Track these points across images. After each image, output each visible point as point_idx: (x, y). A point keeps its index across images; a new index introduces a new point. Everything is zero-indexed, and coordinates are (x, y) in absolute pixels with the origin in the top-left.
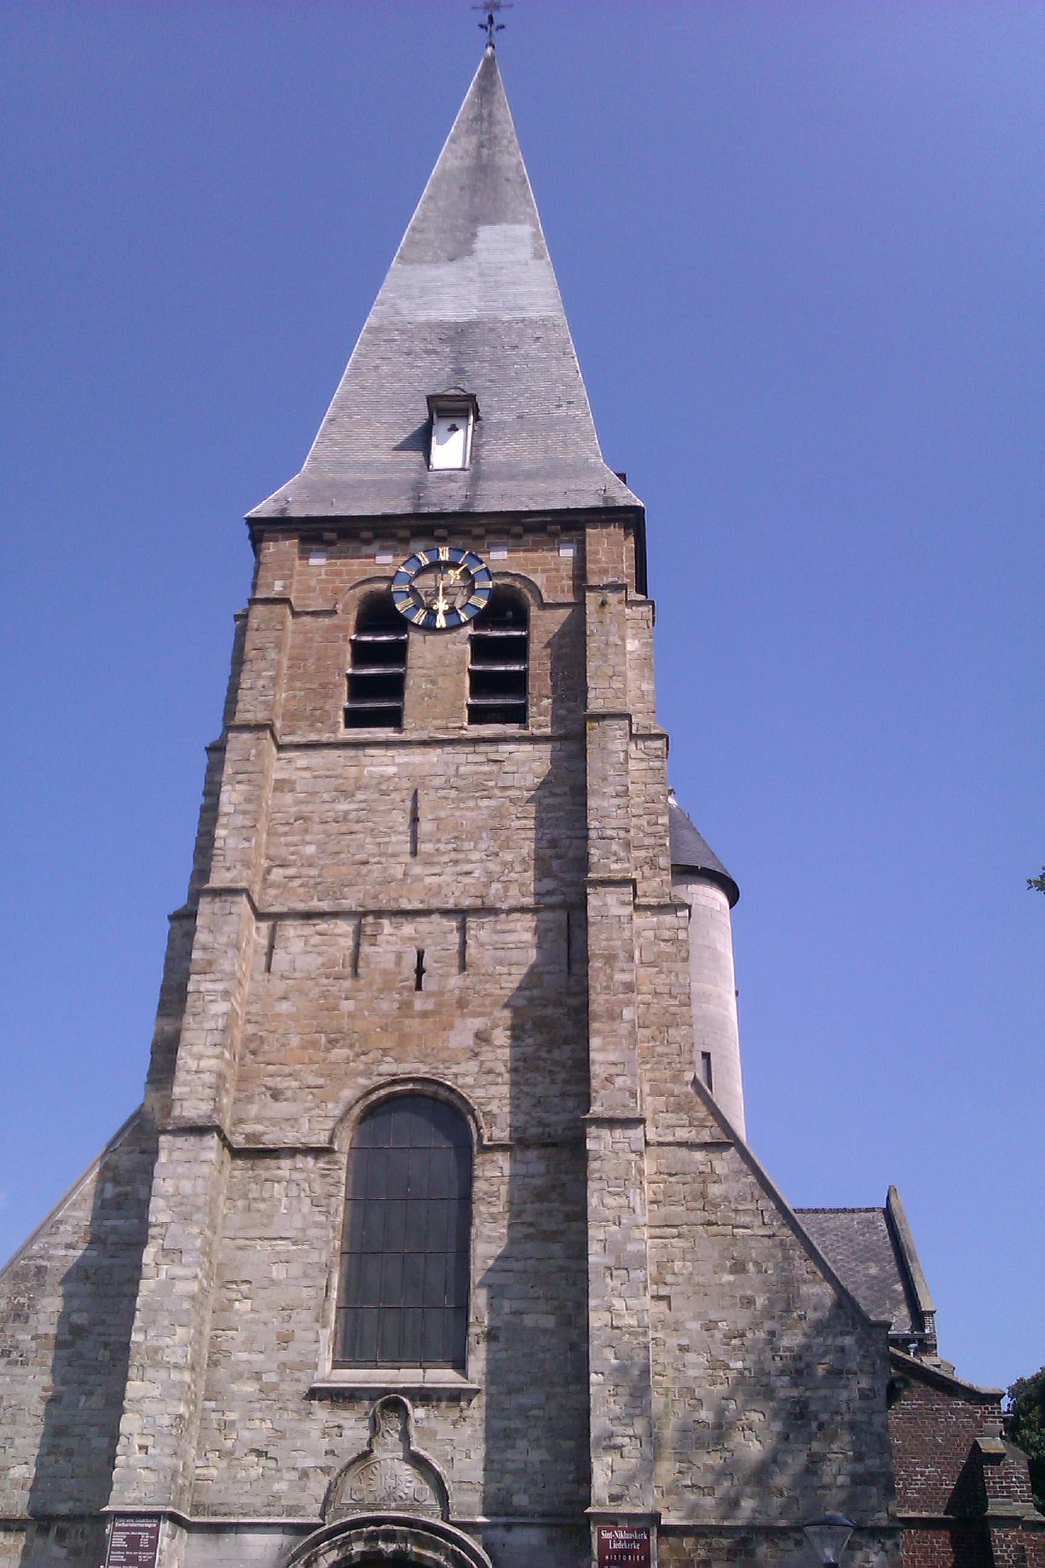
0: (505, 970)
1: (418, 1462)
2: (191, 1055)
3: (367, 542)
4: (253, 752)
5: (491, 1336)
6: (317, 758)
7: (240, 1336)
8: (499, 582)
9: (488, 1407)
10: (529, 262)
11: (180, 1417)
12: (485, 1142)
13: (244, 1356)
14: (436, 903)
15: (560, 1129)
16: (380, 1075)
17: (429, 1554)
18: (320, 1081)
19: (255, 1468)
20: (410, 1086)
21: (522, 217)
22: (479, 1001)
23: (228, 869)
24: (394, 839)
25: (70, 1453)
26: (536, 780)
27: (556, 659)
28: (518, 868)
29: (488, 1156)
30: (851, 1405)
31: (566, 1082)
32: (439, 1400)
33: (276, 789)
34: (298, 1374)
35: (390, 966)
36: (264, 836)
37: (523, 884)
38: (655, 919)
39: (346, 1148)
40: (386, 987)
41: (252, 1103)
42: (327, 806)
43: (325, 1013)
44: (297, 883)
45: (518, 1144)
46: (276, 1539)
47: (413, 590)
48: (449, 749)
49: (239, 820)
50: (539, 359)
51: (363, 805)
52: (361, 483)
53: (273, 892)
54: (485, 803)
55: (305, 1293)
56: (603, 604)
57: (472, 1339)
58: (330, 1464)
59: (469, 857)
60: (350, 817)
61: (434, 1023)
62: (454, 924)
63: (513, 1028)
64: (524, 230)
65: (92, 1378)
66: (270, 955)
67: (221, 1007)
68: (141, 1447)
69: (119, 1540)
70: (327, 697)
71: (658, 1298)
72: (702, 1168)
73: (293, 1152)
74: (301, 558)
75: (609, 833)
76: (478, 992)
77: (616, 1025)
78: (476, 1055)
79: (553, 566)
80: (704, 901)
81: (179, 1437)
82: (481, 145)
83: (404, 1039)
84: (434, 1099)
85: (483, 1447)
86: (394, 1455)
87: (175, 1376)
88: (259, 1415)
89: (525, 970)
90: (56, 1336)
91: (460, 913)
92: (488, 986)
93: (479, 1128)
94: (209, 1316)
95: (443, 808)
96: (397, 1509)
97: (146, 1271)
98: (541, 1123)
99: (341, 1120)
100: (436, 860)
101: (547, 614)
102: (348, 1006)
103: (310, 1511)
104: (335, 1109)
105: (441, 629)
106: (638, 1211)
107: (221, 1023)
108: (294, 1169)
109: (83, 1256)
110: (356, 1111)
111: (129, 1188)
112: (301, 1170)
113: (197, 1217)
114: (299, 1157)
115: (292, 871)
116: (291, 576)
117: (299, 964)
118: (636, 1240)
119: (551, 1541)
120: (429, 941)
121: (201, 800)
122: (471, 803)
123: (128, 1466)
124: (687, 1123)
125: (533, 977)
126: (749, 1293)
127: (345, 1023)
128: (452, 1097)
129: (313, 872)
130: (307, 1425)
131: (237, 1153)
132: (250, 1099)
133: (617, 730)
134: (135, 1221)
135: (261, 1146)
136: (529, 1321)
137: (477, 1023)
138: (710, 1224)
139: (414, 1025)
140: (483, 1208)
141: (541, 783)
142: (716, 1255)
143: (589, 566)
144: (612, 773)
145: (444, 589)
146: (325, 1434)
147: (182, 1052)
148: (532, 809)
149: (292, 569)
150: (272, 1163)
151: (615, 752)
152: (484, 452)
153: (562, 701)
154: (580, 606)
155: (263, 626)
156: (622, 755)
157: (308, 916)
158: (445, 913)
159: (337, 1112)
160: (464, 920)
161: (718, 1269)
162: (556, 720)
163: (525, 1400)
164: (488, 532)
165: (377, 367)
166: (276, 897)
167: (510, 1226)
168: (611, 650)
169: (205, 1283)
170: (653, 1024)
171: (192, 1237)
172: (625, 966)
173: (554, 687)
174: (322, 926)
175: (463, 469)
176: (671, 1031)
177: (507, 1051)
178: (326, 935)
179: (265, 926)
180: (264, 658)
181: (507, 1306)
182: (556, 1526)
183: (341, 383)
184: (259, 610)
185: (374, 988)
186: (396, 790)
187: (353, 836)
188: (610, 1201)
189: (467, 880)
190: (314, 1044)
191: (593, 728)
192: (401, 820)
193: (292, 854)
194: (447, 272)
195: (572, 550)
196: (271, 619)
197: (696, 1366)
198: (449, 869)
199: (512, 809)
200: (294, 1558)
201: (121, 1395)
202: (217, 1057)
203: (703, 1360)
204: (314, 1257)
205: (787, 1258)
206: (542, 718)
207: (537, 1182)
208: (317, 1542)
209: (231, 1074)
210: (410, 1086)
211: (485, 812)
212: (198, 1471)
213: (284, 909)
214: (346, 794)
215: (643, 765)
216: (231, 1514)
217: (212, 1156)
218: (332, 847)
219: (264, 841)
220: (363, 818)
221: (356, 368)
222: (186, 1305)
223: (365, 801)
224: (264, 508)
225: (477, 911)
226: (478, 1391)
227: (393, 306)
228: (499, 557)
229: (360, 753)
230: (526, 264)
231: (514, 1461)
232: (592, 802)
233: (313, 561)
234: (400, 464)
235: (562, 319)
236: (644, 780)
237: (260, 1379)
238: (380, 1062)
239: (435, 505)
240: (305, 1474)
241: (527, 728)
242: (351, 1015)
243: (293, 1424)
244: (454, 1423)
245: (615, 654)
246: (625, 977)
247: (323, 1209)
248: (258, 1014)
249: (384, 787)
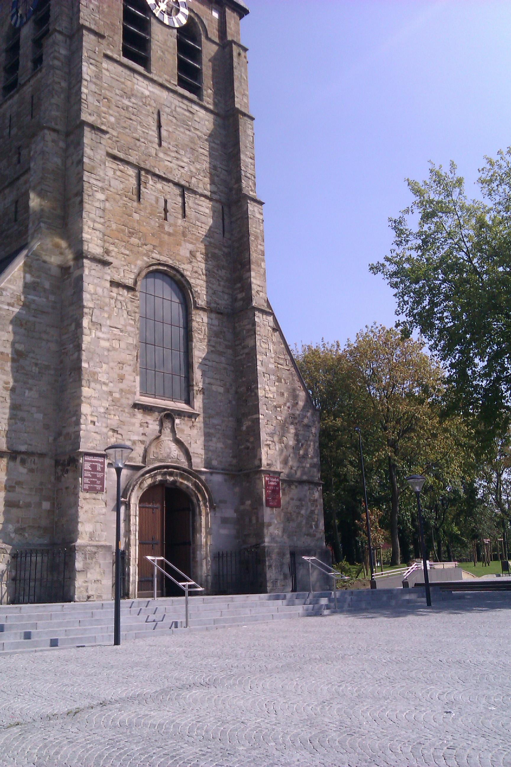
0: (199, 224)
16: (153, 258)
17: (186, 482)
18: (127, 252)
20: (165, 268)
25: (23, 420)
26: (207, 131)
29: (198, 311)
31: (224, 287)
43: (126, 216)
48: (171, 94)
51: (135, 106)
65: (30, 381)
68: (91, 421)
78: (191, 262)
86: (168, 438)
88: (112, 412)
92: (194, 230)
96: (171, 462)
97: (86, 331)
103: (137, 460)
110: (144, 273)
111: (39, 280)
112: (122, 296)
114: (120, 289)
123: (87, 430)
126: (282, 391)
128: (182, 279)
130: (134, 420)
136: (214, 388)
137: (190, 247)
140: (196, 335)
146: (141, 426)
159: (136, 271)
178: (124, 173)
182: (225, 474)
190: (123, 231)
205: (293, 380)
207: (215, 328)
210: (165, 268)
220: (135, 113)
223: (136, 104)
231: (212, 446)
238: (152, 252)
243: (128, 419)
247: (133, 318)
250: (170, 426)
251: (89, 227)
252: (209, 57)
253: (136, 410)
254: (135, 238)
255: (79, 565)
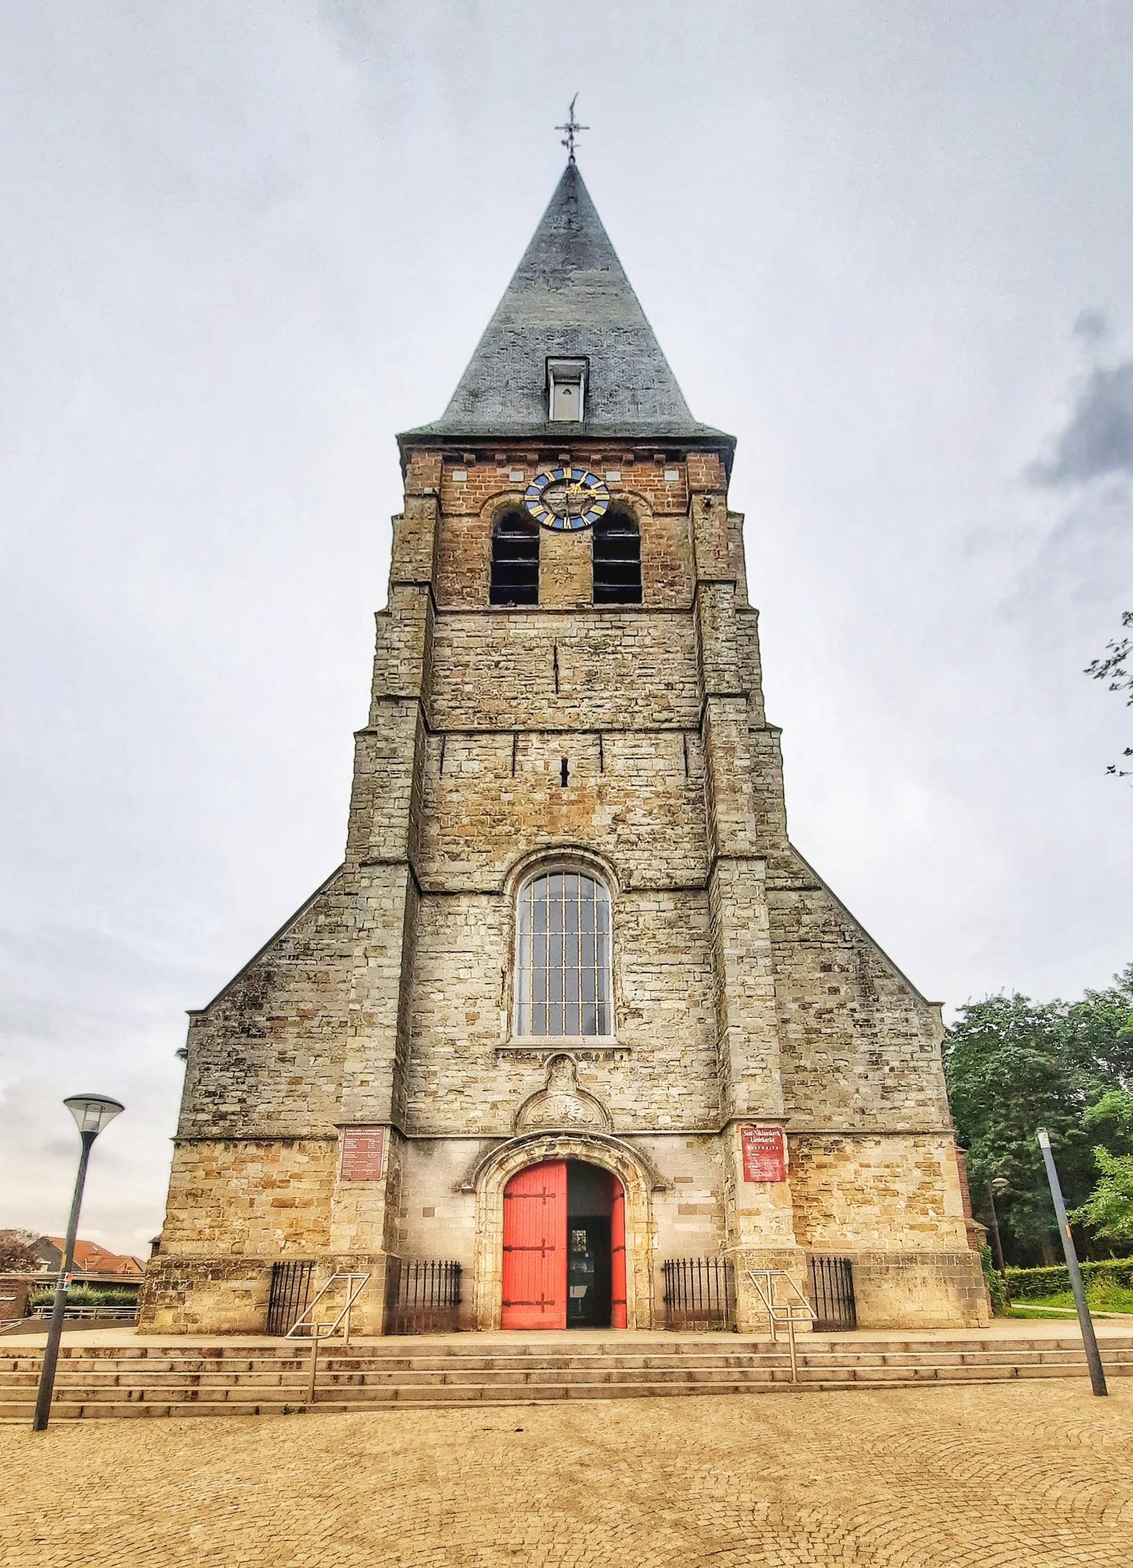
30: (914, 1055)
34: (484, 1041)
60: (500, 665)
126: (835, 985)
127: (507, 809)
157: (470, 733)
197: (795, 1032)
208: (508, 1148)
240: (494, 1106)
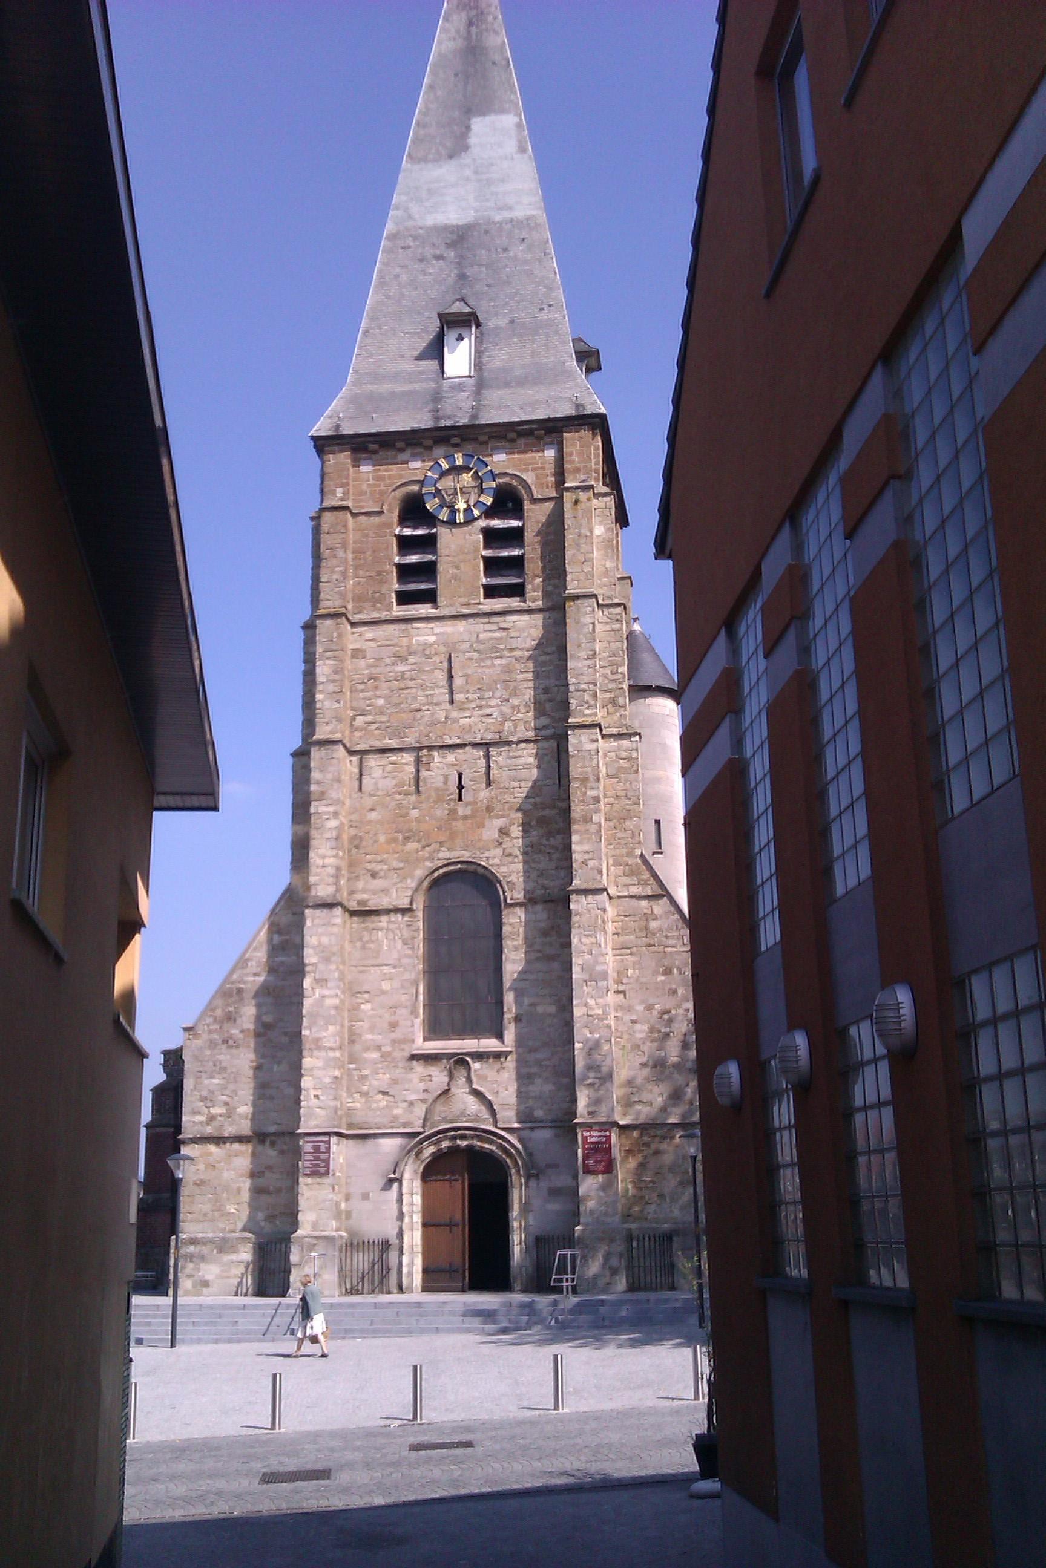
0: (516, 784)
1: (477, 1094)
2: (317, 854)
3: (402, 450)
4: (335, 635)
5: (517, 1019)
6: (380, 631)
7: (366, 1025)
8: (501, 481)
9: (518, 1061)
10: (515, 156)
11: (336, 1078)
12: (509, 901)
13: (369, 1037)
14: (469, 739)
15: (556, 890)
16: (439, 860)
17: (487, 1146)
18: (401, 865)
19: (382, 1101)
20: (459, 866)
21: (508, 106)
22: (500, 807)
23: (327, 723)
24: (437, 692)
25: (272, 1098)
27: (545, 544)
28: (523, 711)
29: (511, 910)
31: (559, 860)
32: (488, 1058)
33: (353, 657)
35: (440, 785)
36: (349, 693)
37: (526, 722)
38: (616, 744)
39: (421, 907)
40: (439, 800)
41: (359, 880)
42: (389, 669)
44: (374, 727)
45: (530, 901)
46: (397, 1142)
47: (438, 491)
48: (471, 621)
49: (331, 687)
50: (526, 262)
52: (393, 394)
53: (357, 734)
54: (498, 662)
55: (404, 998)
56: (576, 502)
57: (506, 1021)
58: (426, 1097)
59: (489, 703)
60: (406, 676)
61: (472, 824)
62: (482, 753)
63: (523, 824)
64: (509, 120)
66: (360, 779)
67: (333, 823)
69: (308, 1148)
70: (382, 582)
71: (618, 992)
72: (646, 911)
73: (388, 912)
74: (354, 466)
75: (583, 686)
76: (499, 801)
77: (588, 826)
78: (501, 843)
79: (540, 465)
80: (657, 709)
81: (336, 1089)
82: (470, 24)
83: (452, 836)
84: (475, 873)
85: (515, 1084)
87: (331, 1054)
89: (530, 784)
90: (254, 1030)
91: (486, 745)
93: (504, 892)
94: (346, 1014)
95: (469, 667)
97: (306, 993)
98: (544, 887)
99: (416, 890)
100: (466, 706)
101: (536, 507)
102: (415, 813)
104: (412, 883)
105: (460, 524)
106: (603, 945)
107: (334, 834)
108: (389, 922)
109: (265, 981)
110: (426, 884)
111: (288, 937)
113: (333, 959)
114: (392, 914)
115: (370, 718)
116: (348, 484)
117: (380, 785)
118: (601, 963)
119: (557, 1136)
120: (465, 766)
121: (302, 667)
122: (488, 663)
123: (309, 1107)
124: (636, 883)
125: (536, 789)
126: (674, 987)
128: (487, 873)
129: (384, 719)
130: (410, 1076)
131: (353, 913)
132: (357, 878)
133: (587, 605)
134: (294, 958)
135: (367, 908)
136: (540, 1009)
137: (499, 823)
138: (650, 945)
139: (459, 825)
141: (537, 645)
142: (654, 964)
143: (567, 466)
144: (584, 640)
145: (461, 489)
146: (421, 1081)
147: (312, 854)
148: (530, 664)
149: (347, 477)
150: (376, 918)
151: (587, 625)
152: (485, 359)
153: (550, 579)
154: (559, 500)
155: (331, 530)
156: (591, 626)
157: (383, 751)
158: (475, 745)
159: (414, 885)
160: (488, 750)
161: (656, 973)
162: (546, 595)
163: (540, 1056)
164: (491, 437)
165: (397, 276)
166: (360, 737)
167: (526, 952)
168: (583, 541)
169: (342, 996)
170: (615, 818)
171: (332, 971)
172: (595, 785)
173: (544, 568)
174: (393, 758)
175: (470, 377)
176: (627, 823)
177: (520, 840)
179: (355, 759)
180: (335, 556)
181: (526, 1001)
182: (555, 1127)
183: (370, 294)
184: (327, 517)
185: (431, 800)
186: (436, 654)
187: (409, 691)
188: (585, 940)
189: (488, 720)
190: (395, 840)
191: (571, 606)
192: (441, 677)
193: (368, 706)
194: (445, 172)
195: (553, 451)
196: (337, 524)
197: (641, 1032)
198: (477, 713)
199: (517, 666)
200: (409, 1151)
201: (299, 1066)
202: (334, 856)
203: (646, 1028)
204: (407, 976)
206: (536, 594)
207: (543, 925)
208: (421, 1142)
209: (344, 864)
210: (459, 866)
211: (499, 669)
212: (349, 1105)
213: (367, 747)
214: (402, 659)
215: (608, 627)
216: (371, 1128)
217: (338, 921)
218: (395, 699)
219: (348, 697)
220: (415, 676)
221: (381, 277)
222: (333, 1012)
223: (415, 664)
224: (322, 427)
225: (496, 744)
226: (511, 1052)
227: (406, 210)
228: (499, 460)
229: (409, 626)
230: (512, 159)
232: (570, 664)
233: (363, 469)
234: (421, 373)
235: (542, 217)
236: (609, 639)
237: (380, 1049)
238: (439, 851)
239: (449, 418)
240: (411, 1104)
241: (525, 602)
242: (417, 820)
244: (498, 1071)
245: (585, 543)
246: (594, 793)
248: (356, 821)
249: (427, 652)
250: (466, 1075)
251: (318, 867)
252: (536, 529)
253: (414, 1062)
254: (413, 842)
255: (294, 1258)
